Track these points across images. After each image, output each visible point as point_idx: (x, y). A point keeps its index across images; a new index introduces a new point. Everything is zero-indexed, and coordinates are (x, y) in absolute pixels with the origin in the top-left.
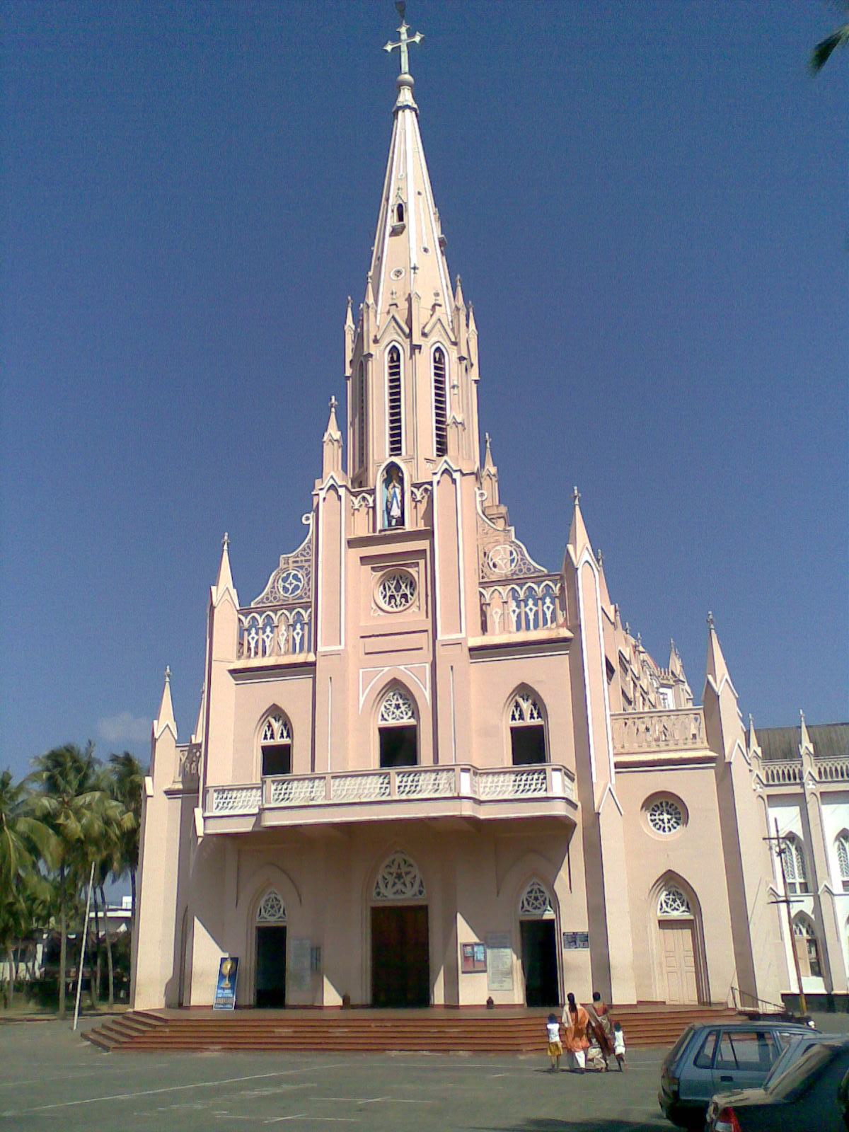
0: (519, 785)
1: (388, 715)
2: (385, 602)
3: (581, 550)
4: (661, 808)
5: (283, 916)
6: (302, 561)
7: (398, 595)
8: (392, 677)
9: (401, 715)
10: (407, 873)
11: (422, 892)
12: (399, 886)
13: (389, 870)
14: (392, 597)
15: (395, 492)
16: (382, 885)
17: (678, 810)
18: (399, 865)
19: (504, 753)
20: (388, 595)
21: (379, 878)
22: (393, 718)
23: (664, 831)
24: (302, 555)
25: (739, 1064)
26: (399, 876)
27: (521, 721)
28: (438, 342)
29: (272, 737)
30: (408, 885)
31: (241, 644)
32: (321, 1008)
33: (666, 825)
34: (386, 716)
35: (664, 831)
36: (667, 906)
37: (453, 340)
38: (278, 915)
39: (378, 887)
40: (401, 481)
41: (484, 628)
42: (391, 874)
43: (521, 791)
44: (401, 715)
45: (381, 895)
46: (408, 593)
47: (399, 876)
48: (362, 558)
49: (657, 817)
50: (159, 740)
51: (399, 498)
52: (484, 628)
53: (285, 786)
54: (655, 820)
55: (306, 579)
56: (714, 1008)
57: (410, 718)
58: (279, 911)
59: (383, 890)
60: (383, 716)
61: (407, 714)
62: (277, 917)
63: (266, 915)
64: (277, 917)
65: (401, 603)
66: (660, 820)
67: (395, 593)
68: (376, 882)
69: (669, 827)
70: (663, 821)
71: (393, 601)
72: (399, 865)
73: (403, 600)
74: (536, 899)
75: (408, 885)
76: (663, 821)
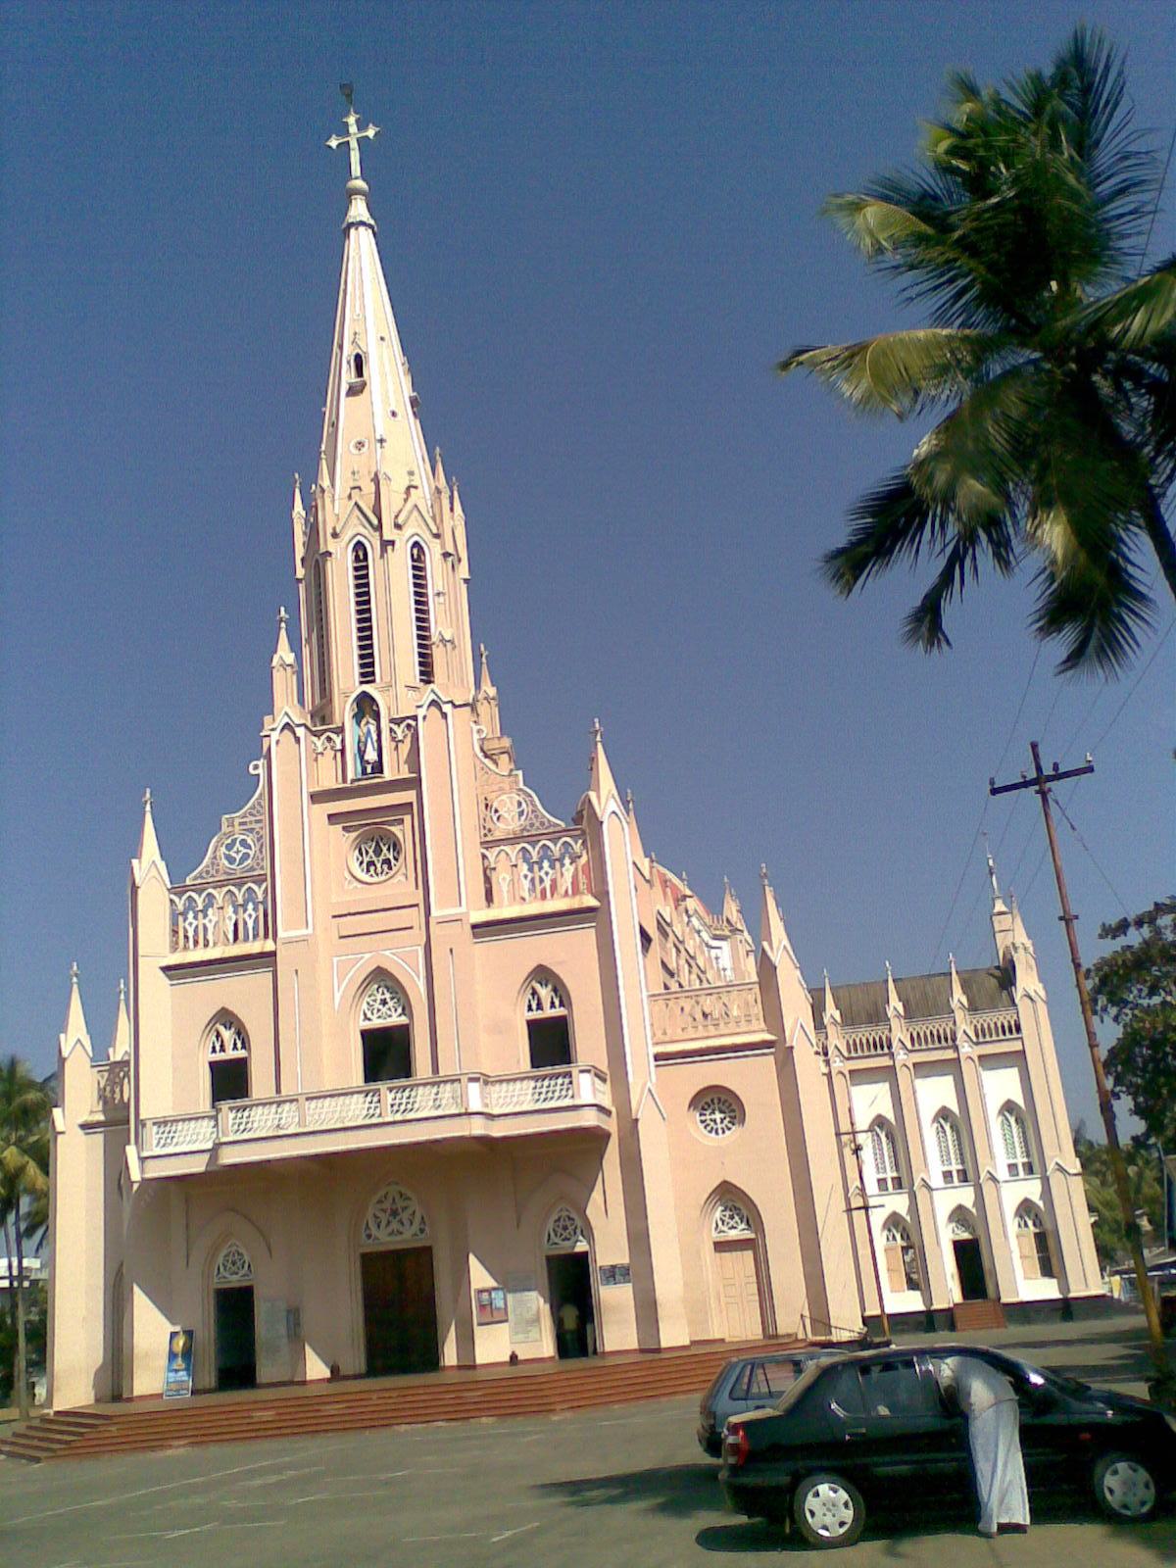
1: (373, 1014)
2: (363, 870)
6: (251, 822)
9: (389, 1013)
10: (404, 1209)
18: (394, 1200)
23: (717, 1133)
24: (251, 814)
26: (394, 1213)
30: (389, 1230)
31: (175, 932)
32: (304, 1383)
33: (719, 1126)
34: (369, 1015)
35: (717, 1133)
40: (377, 716)
44: (389, 1013)
46: (391, 857)
47: (394, 1213)
51: (375, 737)
55: (258, 847)
59: (374, 1231)
60: (365, 1014)
71: (372, 868)
72: (394, 1200)
73: (385, 867)
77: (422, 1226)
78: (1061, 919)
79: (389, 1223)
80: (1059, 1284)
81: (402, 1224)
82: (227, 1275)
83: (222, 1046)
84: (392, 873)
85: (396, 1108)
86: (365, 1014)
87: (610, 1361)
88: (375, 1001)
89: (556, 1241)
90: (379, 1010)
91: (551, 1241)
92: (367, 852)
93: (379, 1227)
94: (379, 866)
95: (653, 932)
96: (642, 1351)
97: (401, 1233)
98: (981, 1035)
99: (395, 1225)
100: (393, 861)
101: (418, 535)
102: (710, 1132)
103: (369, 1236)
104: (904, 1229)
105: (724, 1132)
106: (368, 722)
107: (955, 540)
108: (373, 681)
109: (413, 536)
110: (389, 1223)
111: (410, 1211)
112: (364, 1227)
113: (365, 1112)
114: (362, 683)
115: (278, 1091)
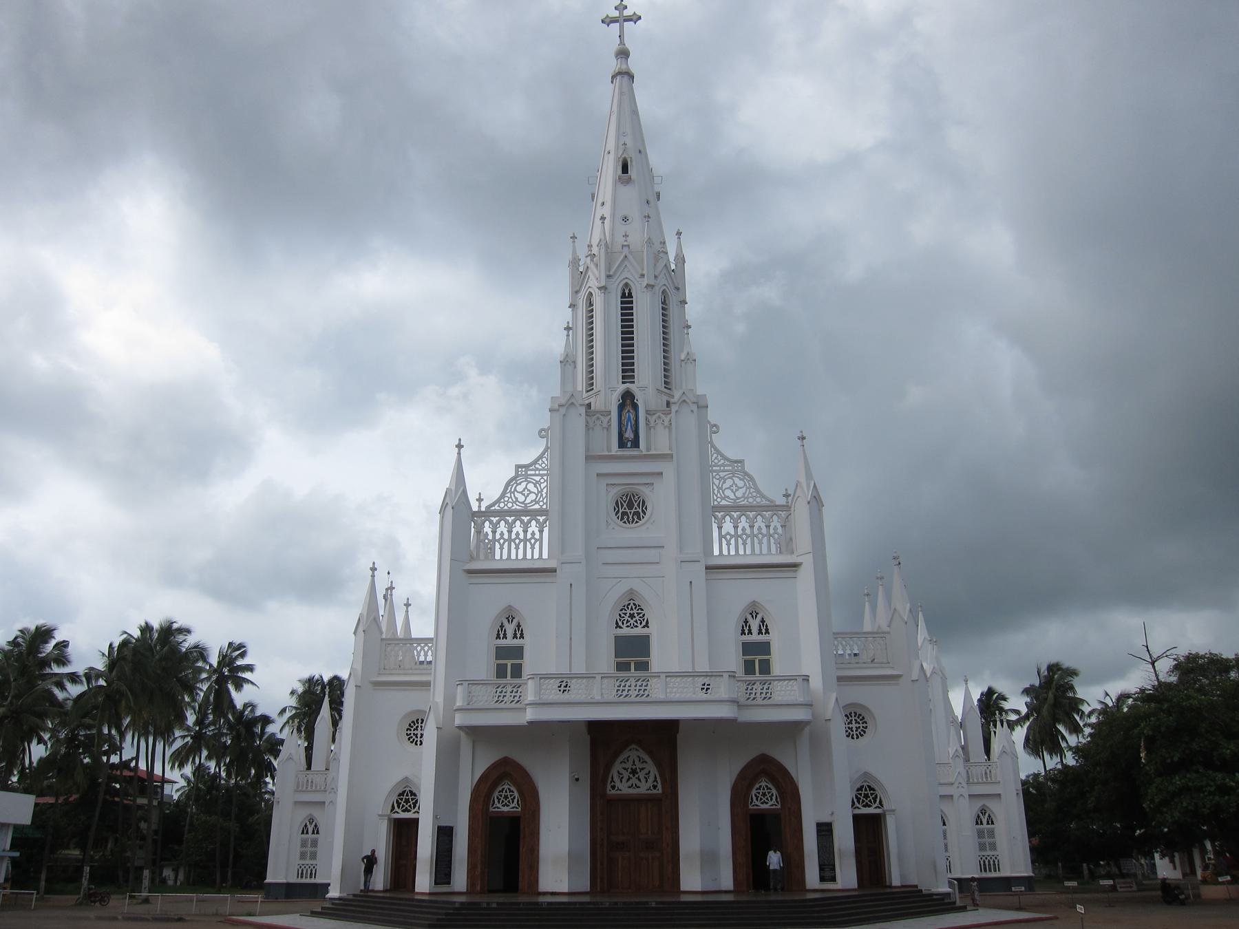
0: (750, 694)
1: (623, 624)
2: (618, 518)
4: (850, 718)
5: (776, 803)
7: (630, 513)
8: (629, 588)
11: (657, 786)
13: (624, 765)
14: (624, 514)
15: (629, 416)
16: (616, 779)
17: (865, 720)
18: (634, 762)
19: (606, 660)
20: (621, 511)
21: (614, 772)
22: (628, 626)
26: (634, 772)
27: (750, 635)
28: (627, 278)
29: (505, 637)
30: (643, 780)
33: (855, 733)
34: (620, 624)
36: (757, 800)
37: (676, 285)
38: (770, 803)
39: (612, 781)
40: (635, 407)
43: (624, 695)
45: (616, 788)
46: (640, 511)
47: (634, 772)
49: (861, 725)
51: (633, 422)
53: (766, 687)
54: (863, 723)
56: (894, 890)
57: (644, 627)
58: (513, 802)
59: (618, 784)
60: (617, 623)
61: (641, 623)
62: (769, 804)
64: (769, 804)
65: (634, 519)
66: (859, 723)
67: (627, 510)
68: (610, 776)
69: (857, 734)
72: (634, 762)
73: (635, 517)
74: (764, 795)
75: (630, 783)
77: (655, 783)
80: (538, 889)
81: (640, 780)
84: (641, 522)
85: (620, 693)
86: (617, 623)
87: (542, 899)
89: (498, 805)
90: (628, 621)
91: (495, 806)
92: (622, 506)
93: (621, 781)
94: (631, 517)
96: (430, 894)
97: (639, 787)
100: (641, 514)
101: (627, 278)
102: (412, 742)
103: (613, 787)
104: (316, 826)
105: (858, 738)
106: (629, 411)
108: (634, 382)
109: (624, 279)
111: (646, 771)
112: (610, 780)
113: (496, 699)
114: (623, 383)
115: (570, 671)
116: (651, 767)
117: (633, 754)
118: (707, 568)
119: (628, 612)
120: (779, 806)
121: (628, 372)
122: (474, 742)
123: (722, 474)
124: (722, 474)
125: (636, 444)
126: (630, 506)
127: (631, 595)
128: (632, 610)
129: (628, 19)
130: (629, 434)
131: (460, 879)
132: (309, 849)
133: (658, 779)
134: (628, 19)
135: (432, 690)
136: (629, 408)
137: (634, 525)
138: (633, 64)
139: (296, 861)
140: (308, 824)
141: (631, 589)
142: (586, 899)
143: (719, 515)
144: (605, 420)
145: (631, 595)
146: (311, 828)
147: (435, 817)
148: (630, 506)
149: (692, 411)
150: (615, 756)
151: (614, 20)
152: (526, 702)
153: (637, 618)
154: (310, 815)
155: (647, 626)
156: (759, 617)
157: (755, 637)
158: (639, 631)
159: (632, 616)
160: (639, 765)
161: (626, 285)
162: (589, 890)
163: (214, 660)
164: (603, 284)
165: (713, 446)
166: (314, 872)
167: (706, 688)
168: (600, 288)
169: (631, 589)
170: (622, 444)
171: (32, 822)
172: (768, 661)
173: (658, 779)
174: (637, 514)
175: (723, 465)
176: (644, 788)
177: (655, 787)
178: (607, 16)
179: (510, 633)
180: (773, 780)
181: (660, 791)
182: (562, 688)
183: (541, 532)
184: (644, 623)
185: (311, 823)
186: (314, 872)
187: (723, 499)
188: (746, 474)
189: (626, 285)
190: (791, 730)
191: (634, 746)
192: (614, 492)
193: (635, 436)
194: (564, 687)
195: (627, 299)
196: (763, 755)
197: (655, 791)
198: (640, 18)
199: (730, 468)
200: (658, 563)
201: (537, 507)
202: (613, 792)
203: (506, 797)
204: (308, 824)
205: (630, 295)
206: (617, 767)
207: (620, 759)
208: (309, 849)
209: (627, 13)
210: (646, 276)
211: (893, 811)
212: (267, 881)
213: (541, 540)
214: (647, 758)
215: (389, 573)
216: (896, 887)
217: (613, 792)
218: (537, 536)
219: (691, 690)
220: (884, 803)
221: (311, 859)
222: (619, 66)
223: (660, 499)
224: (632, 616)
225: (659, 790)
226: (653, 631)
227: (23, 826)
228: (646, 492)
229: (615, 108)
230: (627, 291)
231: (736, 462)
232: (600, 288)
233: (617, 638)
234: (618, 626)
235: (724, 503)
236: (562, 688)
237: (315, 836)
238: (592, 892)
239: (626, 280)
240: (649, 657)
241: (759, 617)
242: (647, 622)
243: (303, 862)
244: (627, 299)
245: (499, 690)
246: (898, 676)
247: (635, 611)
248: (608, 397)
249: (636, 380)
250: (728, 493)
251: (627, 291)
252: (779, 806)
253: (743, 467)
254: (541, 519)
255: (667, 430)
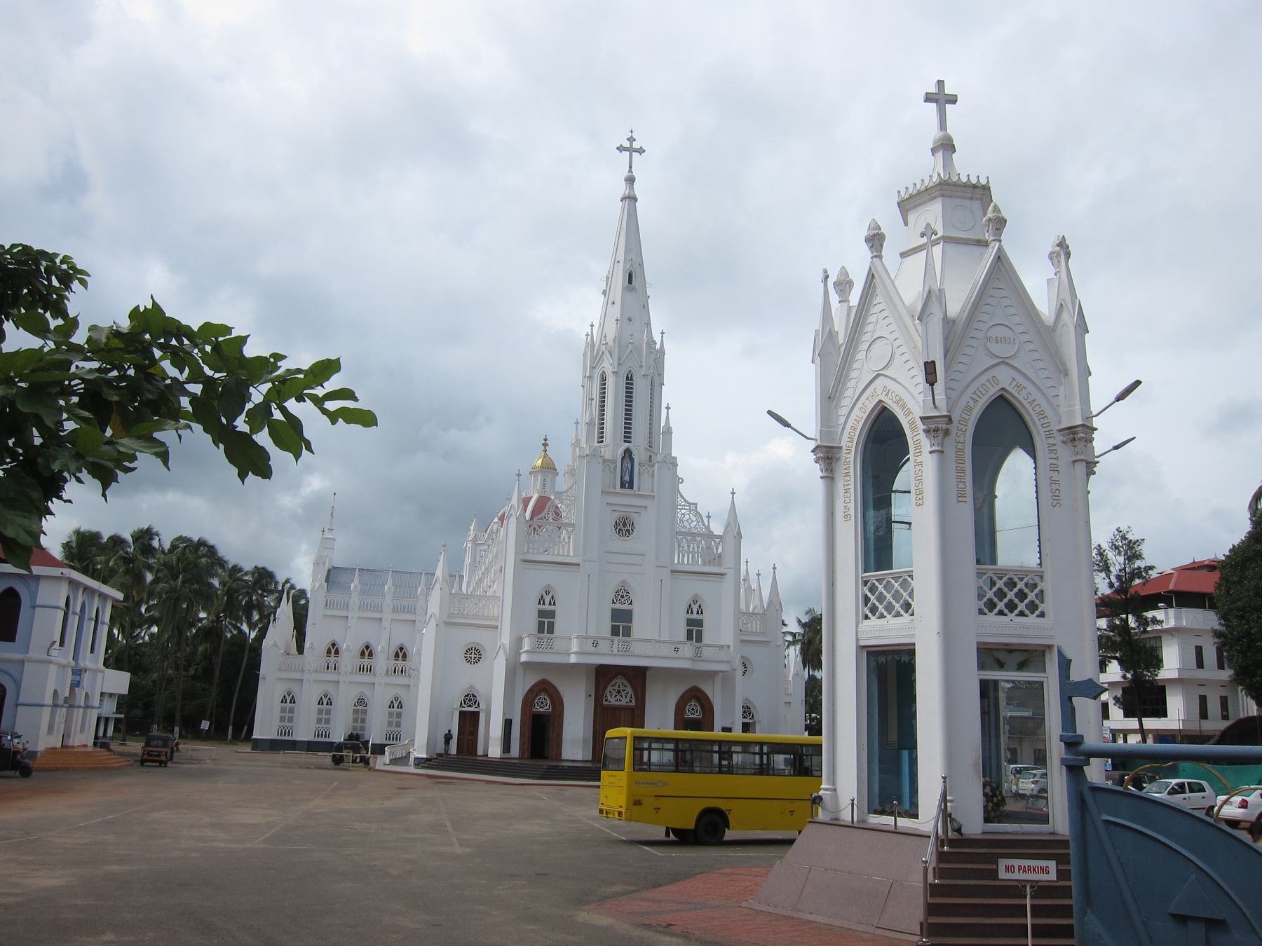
3: (663, 424)
10: (623, 690)
12: (619, 697)
13: (613, 687)
14: (620, 530)
16: (609, 696)
21: (607, 691)
23: (471, 663)
25: (72, 709)
26: (619, 692)
30: (624, 697)
34: (615, 601)
35: (471, 663)
39: (606, 696)
40: (632, 460)
41: (1010, 385)
42: (615, 690)
47: (619, 692)
48: (81, 732)
50: (1048, 569)
52: (1010, 385)
59: (609, 698)
60: (613, 601)
63: (689, 714)
70: (475, 658)
71: (621, 533)
76: (471, 658)
78: (953, 100)
79: (616, 695)
82: (689, 714)
83: (702, 612)
86: (613, 601)
88: (627, 596)
95: (1054, 448)
96: (501, 758)
98: (395, 610)
99: (619, 697)
101: (630, 367)
103: (606, 700)
107: (18, 899)
110: (616, 695)
116: (629, 690)
117: (620, 681)
118: (672, 571)
119: (620, 594)
120: (701, 716)
121: (628, 437)
122: (524, 668)
123: (683, 511)
124: (683, 511)
125: (631, 487)
126: (624, 525)
127: (624, 583)
128: (623, 593)
129: (636, 151)
130: (627, 478)
131: (515, 750)
132: (287, 715)
133: (633, 697)
134: (636, 151)
135: (499, 631)
136: (628, 459)
137: (626, 538)
138: (638, 189)
139: (313, 726)
140: (287, 695)
141: (624, 580)
142: (589, 765)
143: (680, 537)
144: (612, 466)
145: (624, 583)
146: (289, 699)
147: (504, 714)
148: (624, 525)
149: (669, 469)
150: (610, 681)
151: (626, 149)
152: (572, 651)
153: (624, 594)
154: (289, 688)
155: (631, 603)
156: (698, 604)
157: (695, 616)
158: (626, 607)
159: (622, 597)
160: (622, 688)
161: (630, 371)
162: (591, 759)
163: (230, 566)
164: (615, 370)
165: (679, 492)
166: (328, 733)
167: (676, 650)
168: (613, 372)
169: (624, 580)
170: (622, 486)
171: (129, 692)
172: (701, 631)
173: (633, 697)
174: (628, 531)
175: (684, 505)
176: (624, 702)
177: (631, 701)
178: (621, 145)
179: (547, 602)
180: (699, 700)
181: (634, 704)
182: (595, 645)
183: (569, 538)
184: (629, 602)
185: (289, 695)
186: (328, 733)
187: (682, 527)
188: (698, 513)
189: (630, 371)
190: (712, 675)
191: (620, 677)
192: (616, 516)
193: (630, 479)
194: (595, 644)
195: (629, 380)
196: (695, 687)
197: (630, 704)
198: (644, 151)
199: (688, 508)
200: (640, 565)
201: (567, 521)
202: (606, 703)
203: (542, 703)
204: (287, 695)
205: (632, 379)
206: (609, 688)
207: (612, 683)
208: (324, 716)
209: (636, 145)
210: (644, 368)
211: (760, 721)
212: (253, 737)
213: (569, 542)
214: (627, 684)
215: (335, 494)
216: (479, 756)
217: (606, 703)
218: (567, 540)
219: (667, 650)
220: (755, 716)
221: (288, 721)
222: (627, 192)
223: (645, 524)
224: (622, 597)
225: (633, 703)
226: (636, 608)
227: (124, 695)
228: (635, 517)
229: (624, 226)
230: (630, 376)
231: (693, 504)
232: (613, 372)
233: (613, 610)
234: (613, 602)
235: (683, 530)
236: (595, 645)
237: (292, 705)
238: (593, 761)
239: (630, 369)
240: (631, 623)
241: (698, 604)
242: (631, 601)
243: (283, 724)
244: (629, 380)
245: (540, 640)
246: (769, 642)
247: (620, 594)
248: (612, 448)
249: (632, 440)
250: (686, 524)
251: (630, 376)
252: (701, 716)
253: (696, 507)
254: (570, 529)
255: (650, 477)
